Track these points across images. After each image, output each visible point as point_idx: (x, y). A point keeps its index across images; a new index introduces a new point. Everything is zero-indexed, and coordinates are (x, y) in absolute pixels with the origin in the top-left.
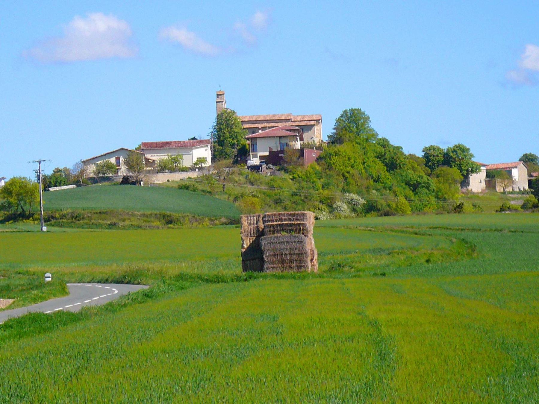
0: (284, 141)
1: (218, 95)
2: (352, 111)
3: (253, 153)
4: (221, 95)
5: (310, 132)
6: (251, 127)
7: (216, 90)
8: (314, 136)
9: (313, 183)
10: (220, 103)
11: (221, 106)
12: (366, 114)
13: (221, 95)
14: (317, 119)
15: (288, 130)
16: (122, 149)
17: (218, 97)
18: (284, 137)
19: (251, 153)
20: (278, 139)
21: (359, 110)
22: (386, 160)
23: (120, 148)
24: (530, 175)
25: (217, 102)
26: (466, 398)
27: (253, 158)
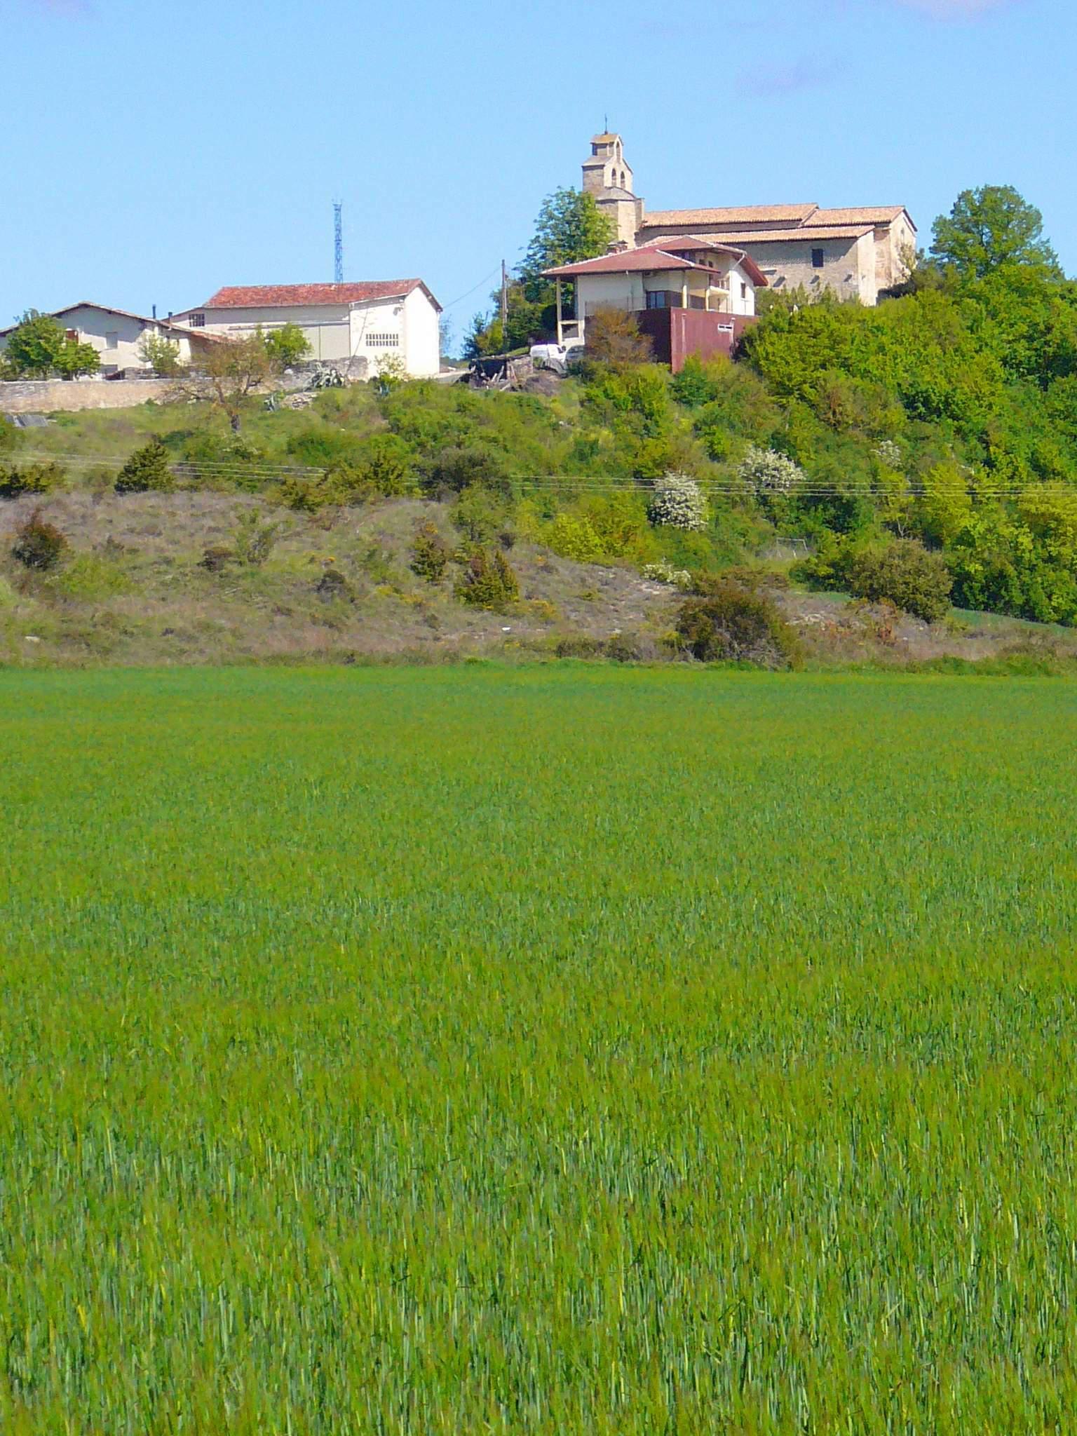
0: (657, 285)
1: (596, 147)
2: (989, 191)
3: (566, 322)
4: (604, 146)
5: (844, 260)
6: (806, 237)
7: (594, 132)
8: (856, 272)
9: (649, 416)
10: (596, 172)
11: (596, 180)
12: (1027, 204)
13: (604, 146)
14: (880, 220)
15: (673, 252)
16: (85, 306)
17: (595, 153)
18: (657, 271)
19: (560, 324)
20: (638, 281)
21: (1007, 192)
22: (1047, 349)
23: (75, 304)
24: (645, 361)
25: (585, 168)
26: (833, 1207)
27: (564, 337)
